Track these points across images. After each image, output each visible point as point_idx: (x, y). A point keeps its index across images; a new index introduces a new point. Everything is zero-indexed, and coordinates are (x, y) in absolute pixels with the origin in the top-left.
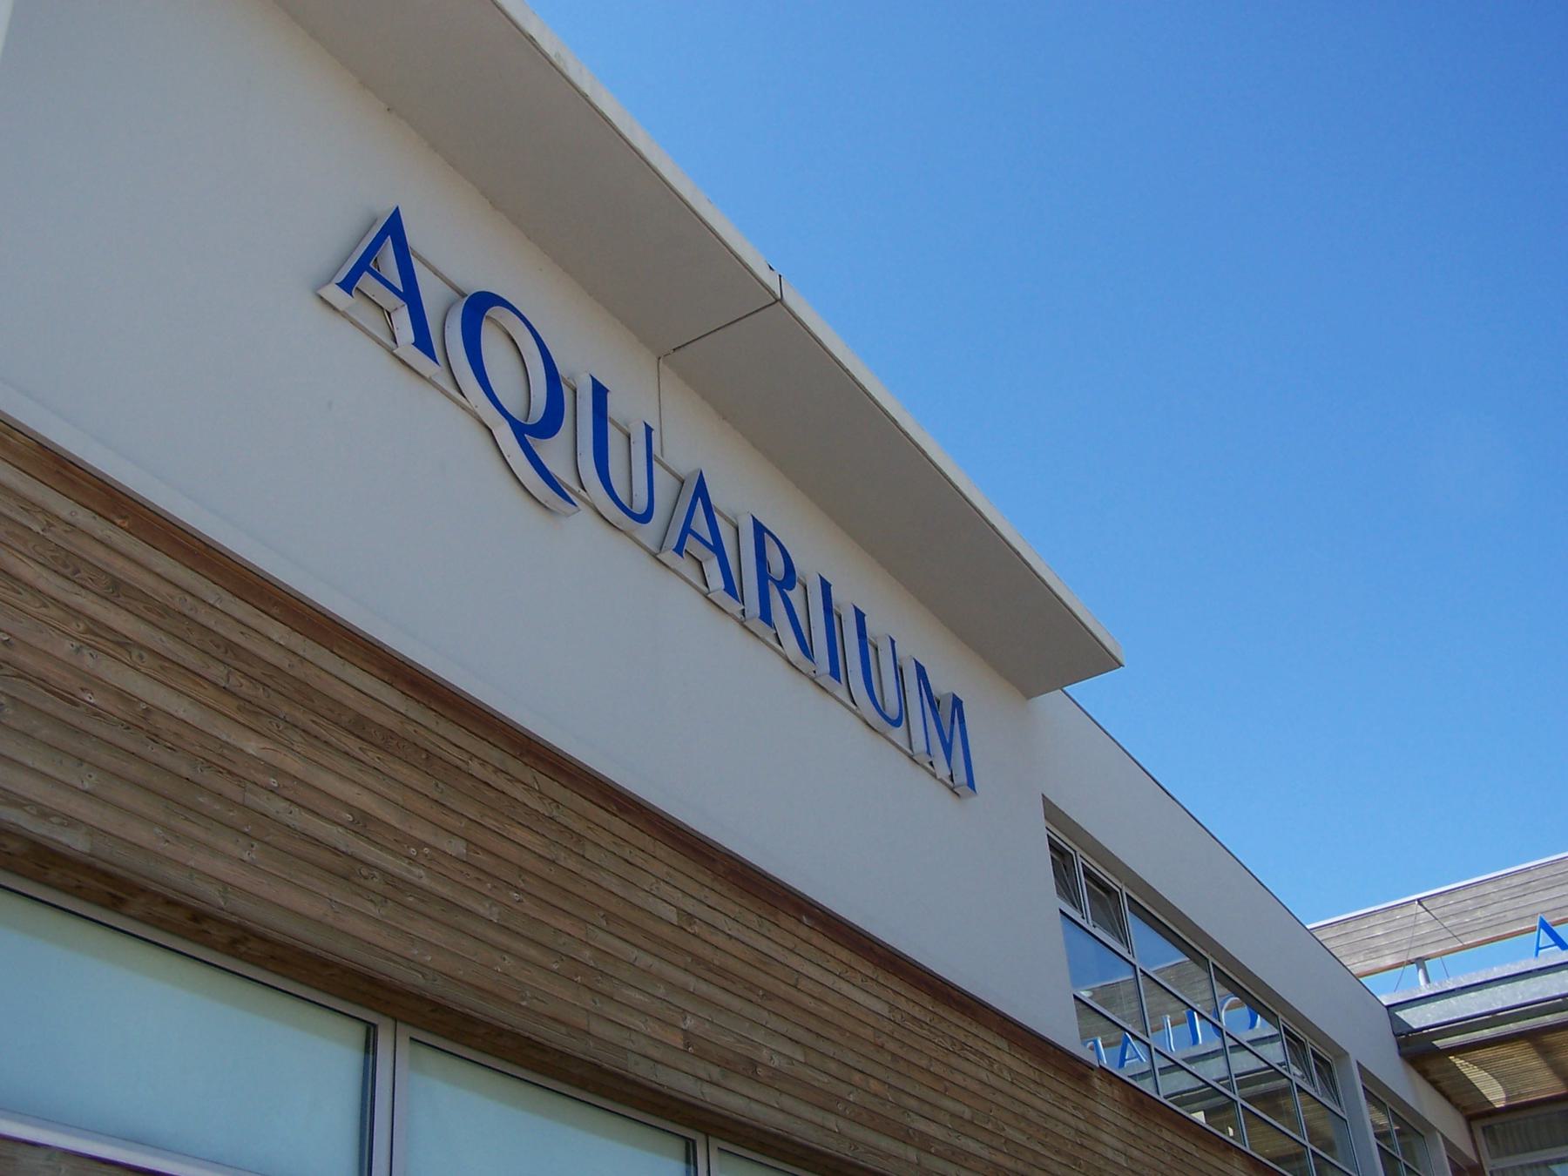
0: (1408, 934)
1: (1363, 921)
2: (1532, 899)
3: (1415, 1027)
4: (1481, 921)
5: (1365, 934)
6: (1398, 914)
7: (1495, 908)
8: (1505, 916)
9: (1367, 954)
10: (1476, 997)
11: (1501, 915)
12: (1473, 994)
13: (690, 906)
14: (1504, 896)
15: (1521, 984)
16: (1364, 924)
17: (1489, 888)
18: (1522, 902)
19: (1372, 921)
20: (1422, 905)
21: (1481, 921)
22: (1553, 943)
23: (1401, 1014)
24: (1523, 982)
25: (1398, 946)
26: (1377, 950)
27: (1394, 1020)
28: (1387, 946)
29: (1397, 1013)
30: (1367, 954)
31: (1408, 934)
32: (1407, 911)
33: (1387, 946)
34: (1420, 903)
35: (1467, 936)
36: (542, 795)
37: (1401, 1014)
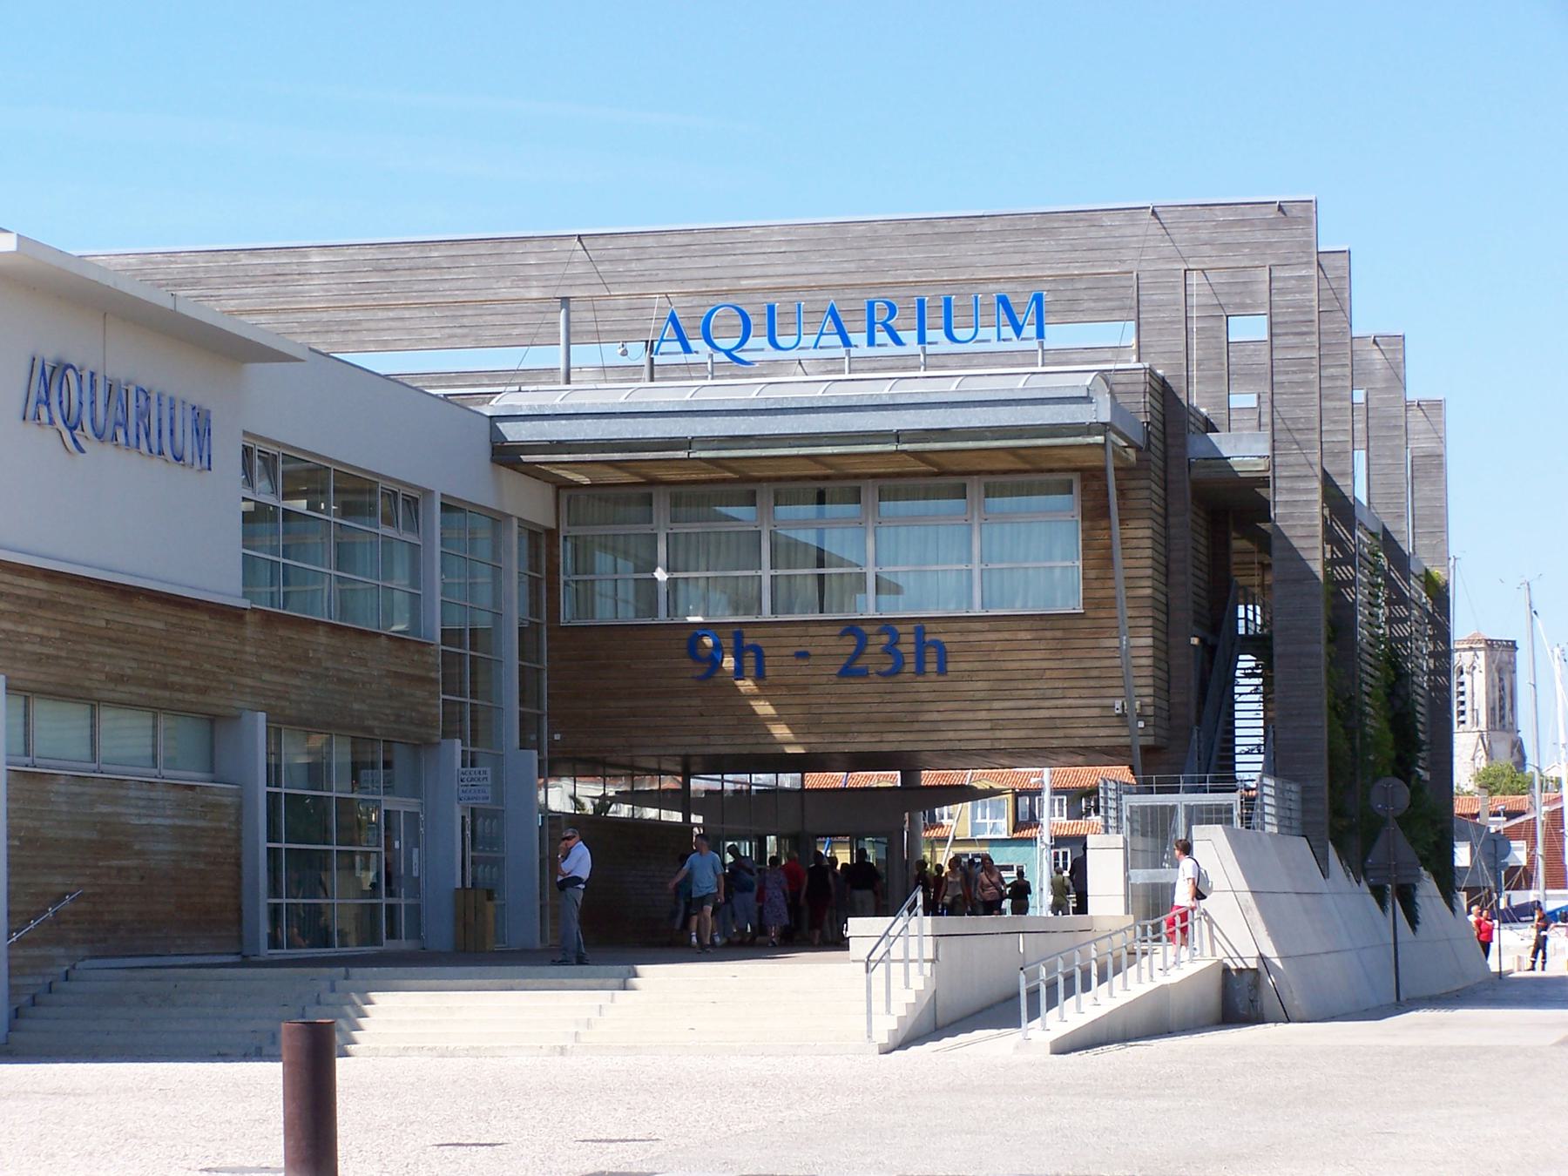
0: (560, 270)
1: (519, 245)
2: (687, 263)
3: (509, 439)
4: (634, 273)
5: (517, 259)
6: (556, 246)
7: (649, 264)
8: (657, 275)
9: (514, 280)
10: (565, 425)
11: (654, 272)
12: (563, 422)
13: (108, 616)
14: (662, 253)
15: (604, 422)
16: (520, 248)
17: (650, 241)
18: (676, 264)
19: (529, 246)
20: (581, 242)
21: (634, 273)
22: (676, 338)
23: (501, 426)
24: (606, 421)
25: (547, 280)
26: (526, 279)
27: (496, 435)
28: (536, 278)
29: (498, 424)
30: (514, 280)
31: (560, 270)
32: (566, 245)
33: (536, 278)
34: (579, 239)
35: (617, 286)
36: (75, 597)
37: (501, 426)
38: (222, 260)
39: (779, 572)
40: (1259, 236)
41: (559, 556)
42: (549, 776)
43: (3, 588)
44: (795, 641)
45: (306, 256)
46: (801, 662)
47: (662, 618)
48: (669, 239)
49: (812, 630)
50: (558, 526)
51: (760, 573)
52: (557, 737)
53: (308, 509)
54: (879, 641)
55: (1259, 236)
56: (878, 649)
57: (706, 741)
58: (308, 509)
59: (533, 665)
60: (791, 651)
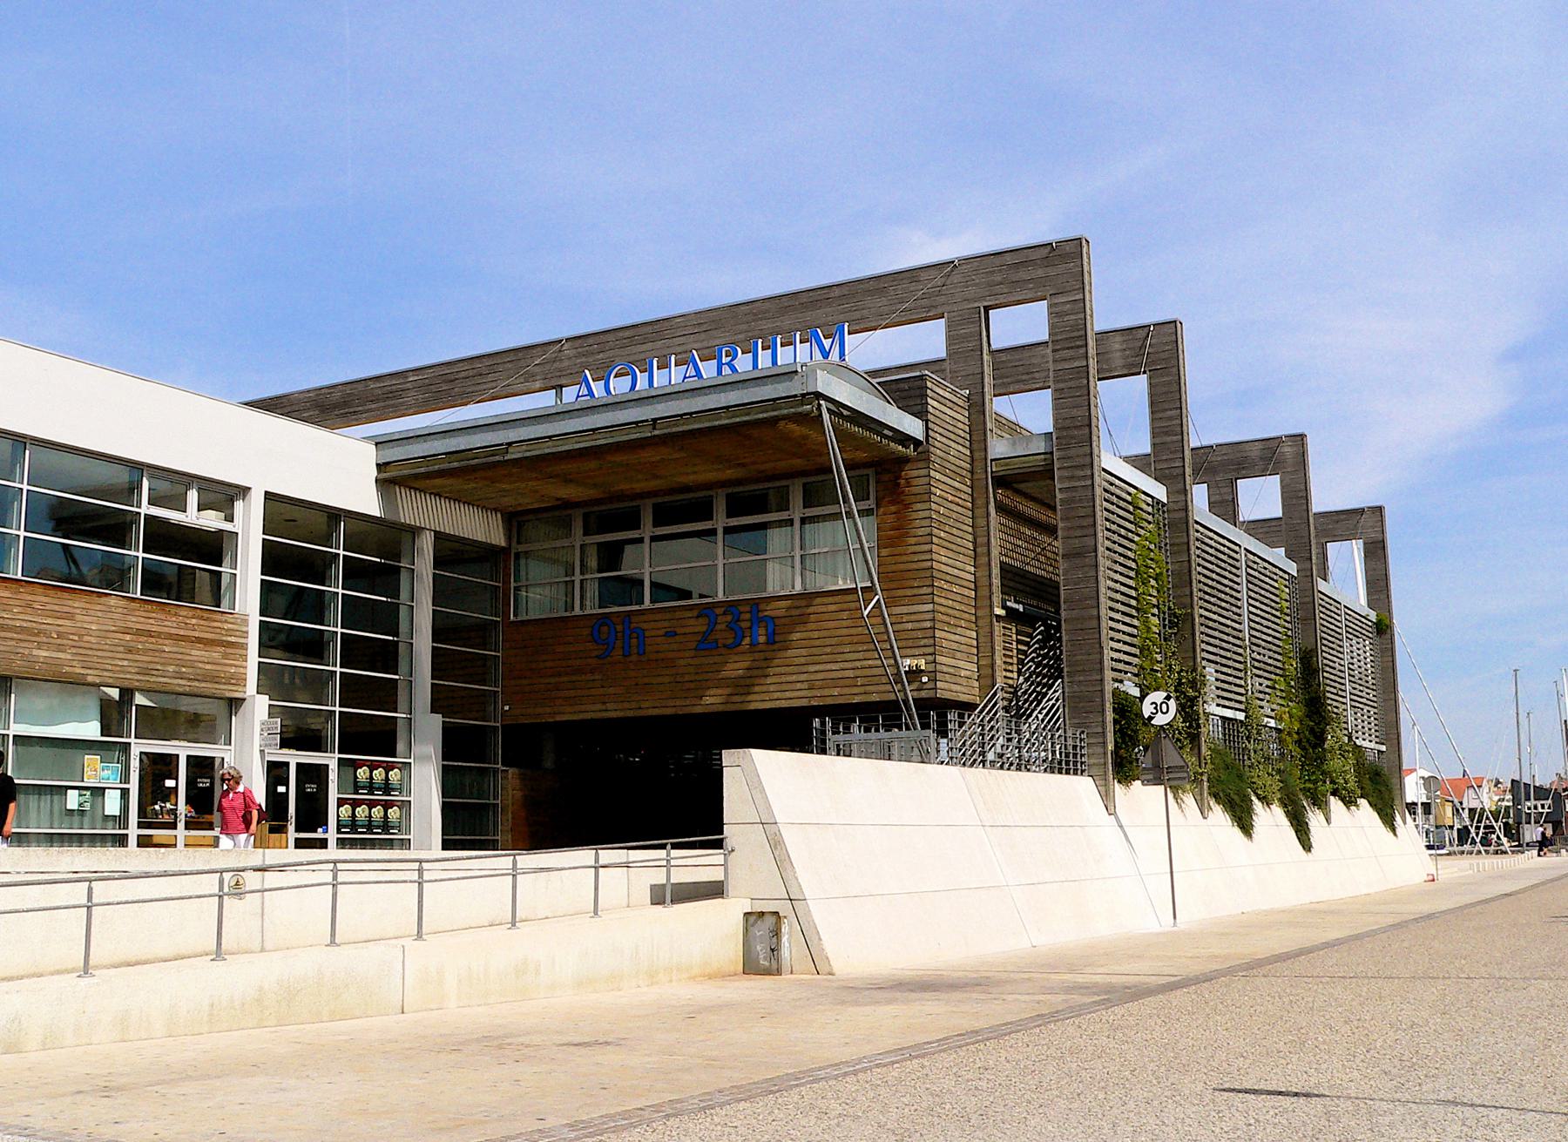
38: (360, 387)
39: (586, 577)
40: (1040, 272)
41: (510, 569)
42: (664, 885)
43: (2, 648)
44: (666, 624)
45: (407, 377)
46: (671, 640)
47: (577, 611)
48: (621, 334)
49: (678, 614)
50: (510, 545)
51: (573, 578)
52: (507, 708)
53: (102, 735)
54: (723, 621)
55: (1040, 272)
56: (723, 626)
57: (604, 707)
58: (102, 735)
59: (493, 653)
60: (662, 632)
